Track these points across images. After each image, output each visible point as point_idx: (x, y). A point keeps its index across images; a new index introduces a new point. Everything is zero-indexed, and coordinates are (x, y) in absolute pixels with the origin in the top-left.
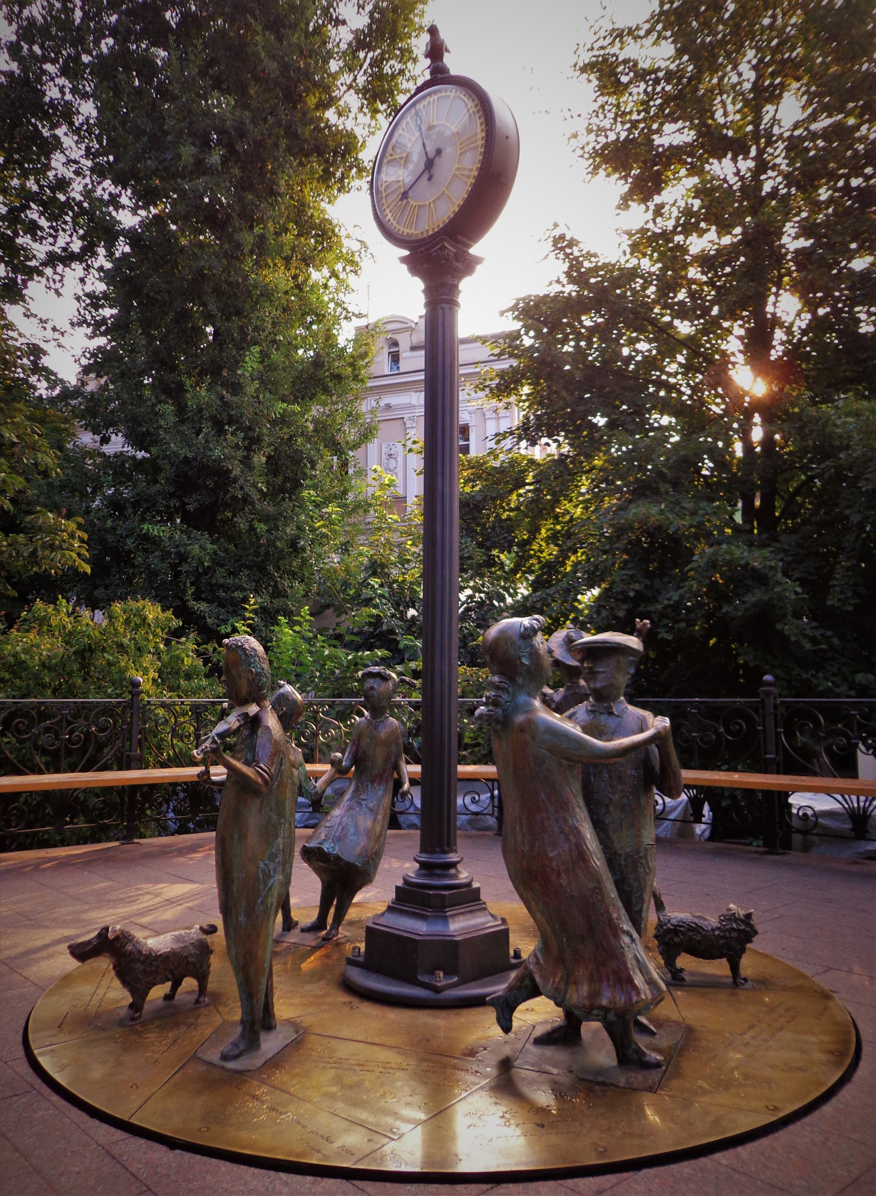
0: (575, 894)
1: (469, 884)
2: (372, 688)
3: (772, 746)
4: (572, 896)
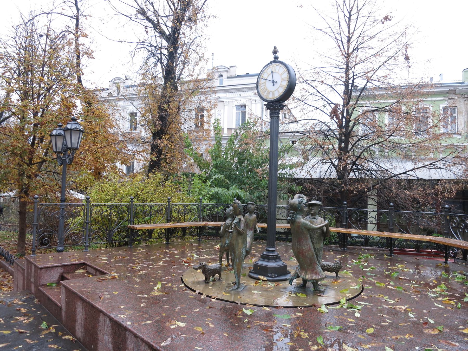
1: (278, 255)
2: (250, 207)
3: (345, 221)
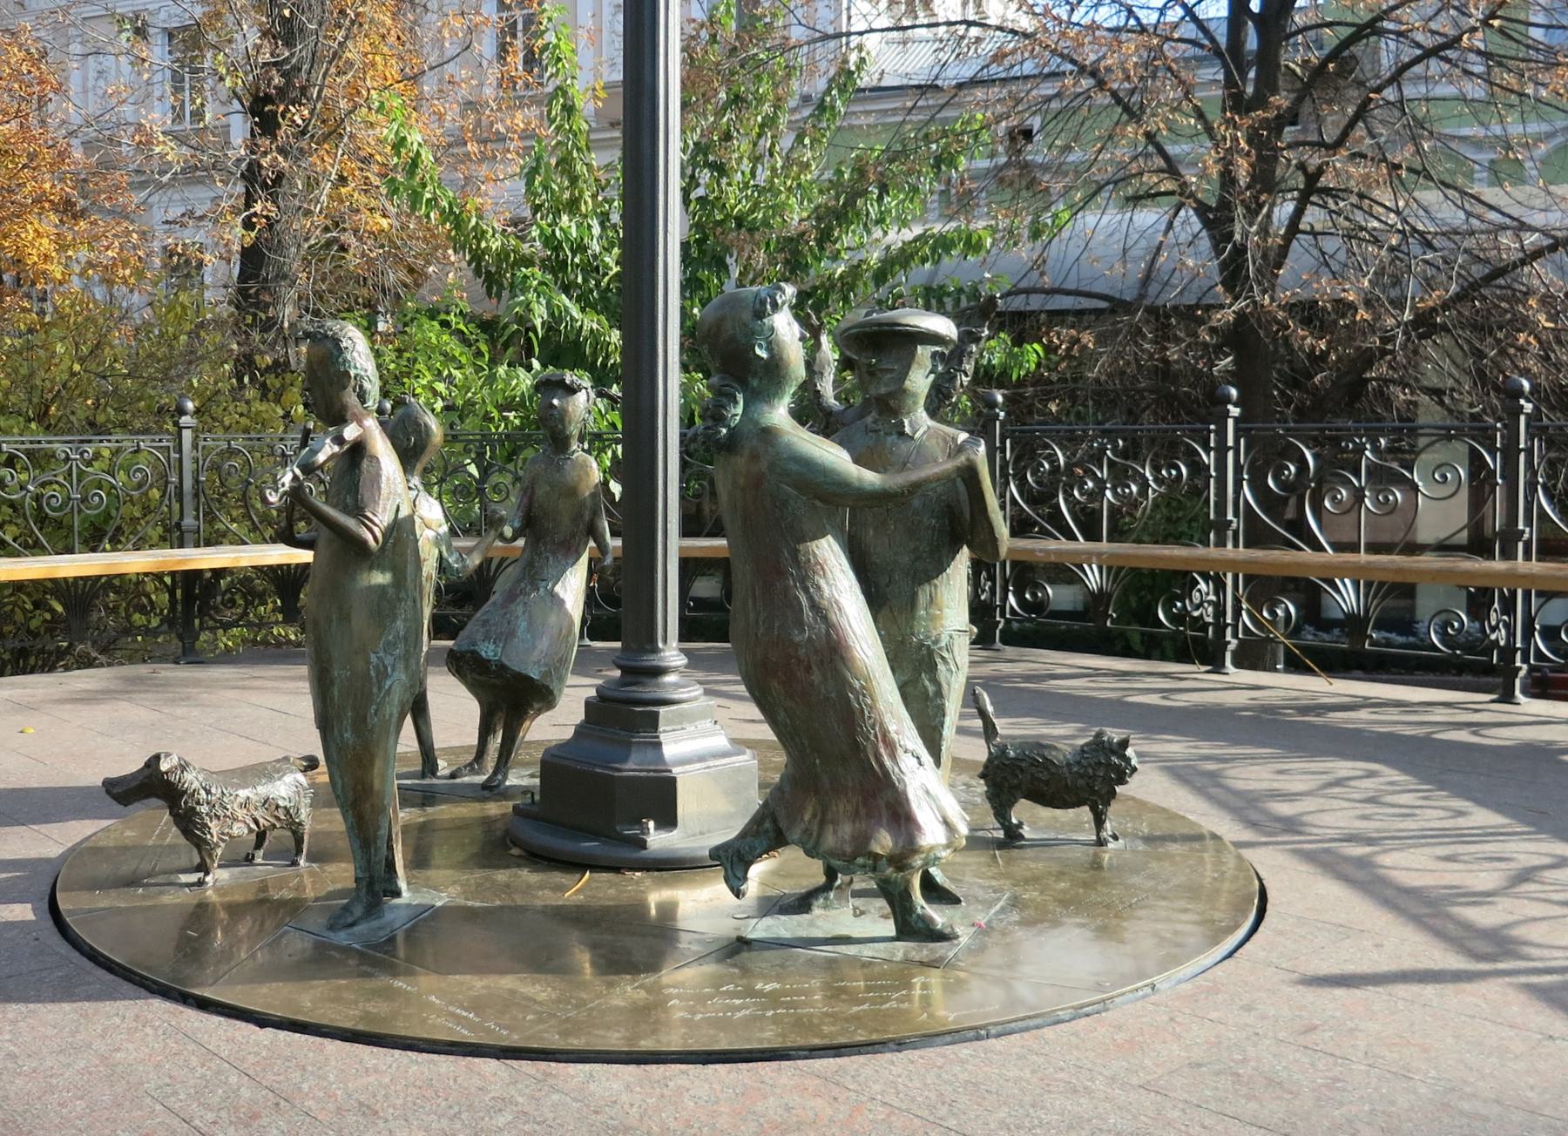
0: (833, 695)
4: (828, 699)
